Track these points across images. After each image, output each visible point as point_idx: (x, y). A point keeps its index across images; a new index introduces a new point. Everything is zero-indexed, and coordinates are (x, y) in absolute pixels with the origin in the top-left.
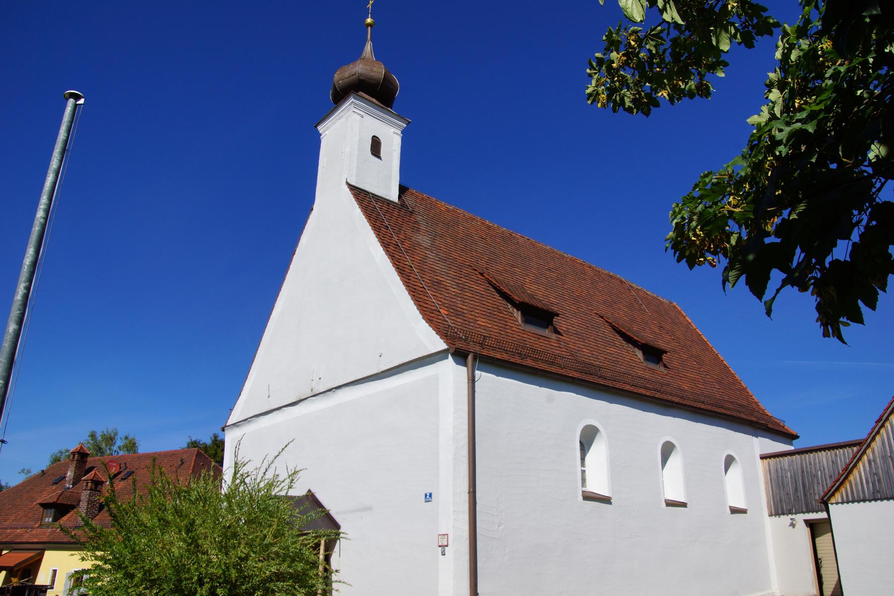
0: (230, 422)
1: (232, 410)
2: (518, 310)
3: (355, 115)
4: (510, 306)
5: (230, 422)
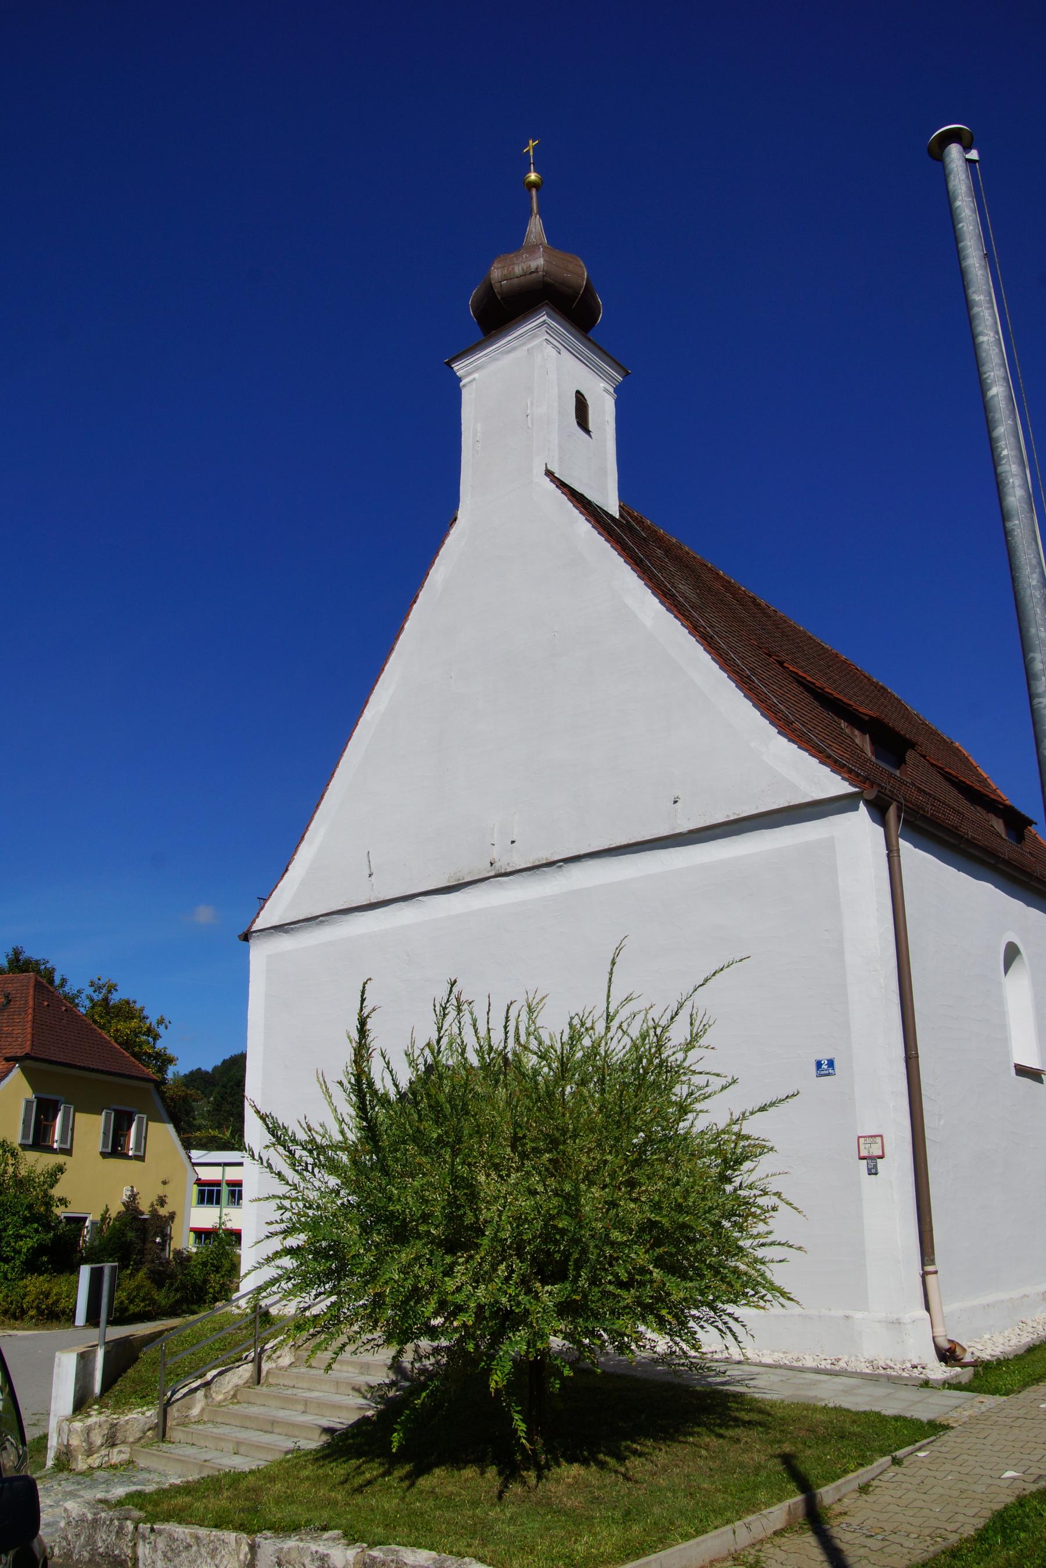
0: (259, 924)
1: (266, 900)
2: (863, 732)
3: (549, 348)
4: (843, 724)
5: (259, 924)
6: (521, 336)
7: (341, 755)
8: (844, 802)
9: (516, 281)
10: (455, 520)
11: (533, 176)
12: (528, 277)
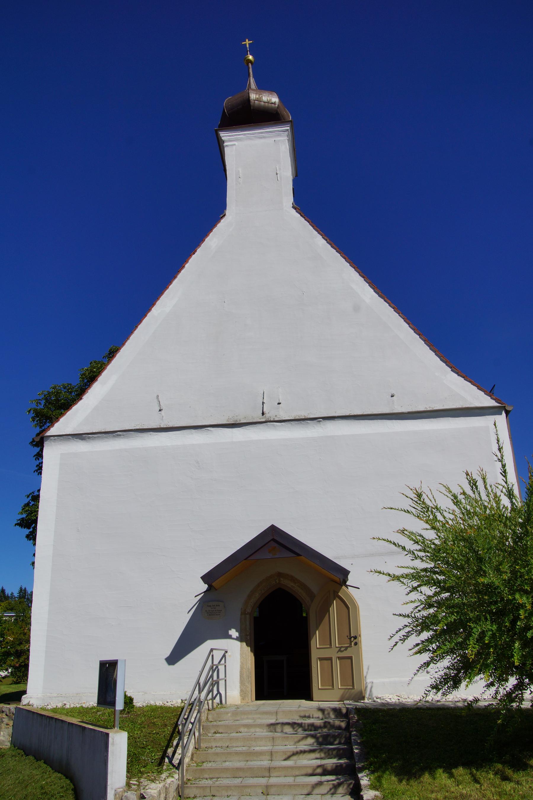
6: (245, 135)
7: (132, 333)
8: (496, 410)
9: (263, 103)
10: (225, 215)
11: (251, 57)
12: (270, 105)
